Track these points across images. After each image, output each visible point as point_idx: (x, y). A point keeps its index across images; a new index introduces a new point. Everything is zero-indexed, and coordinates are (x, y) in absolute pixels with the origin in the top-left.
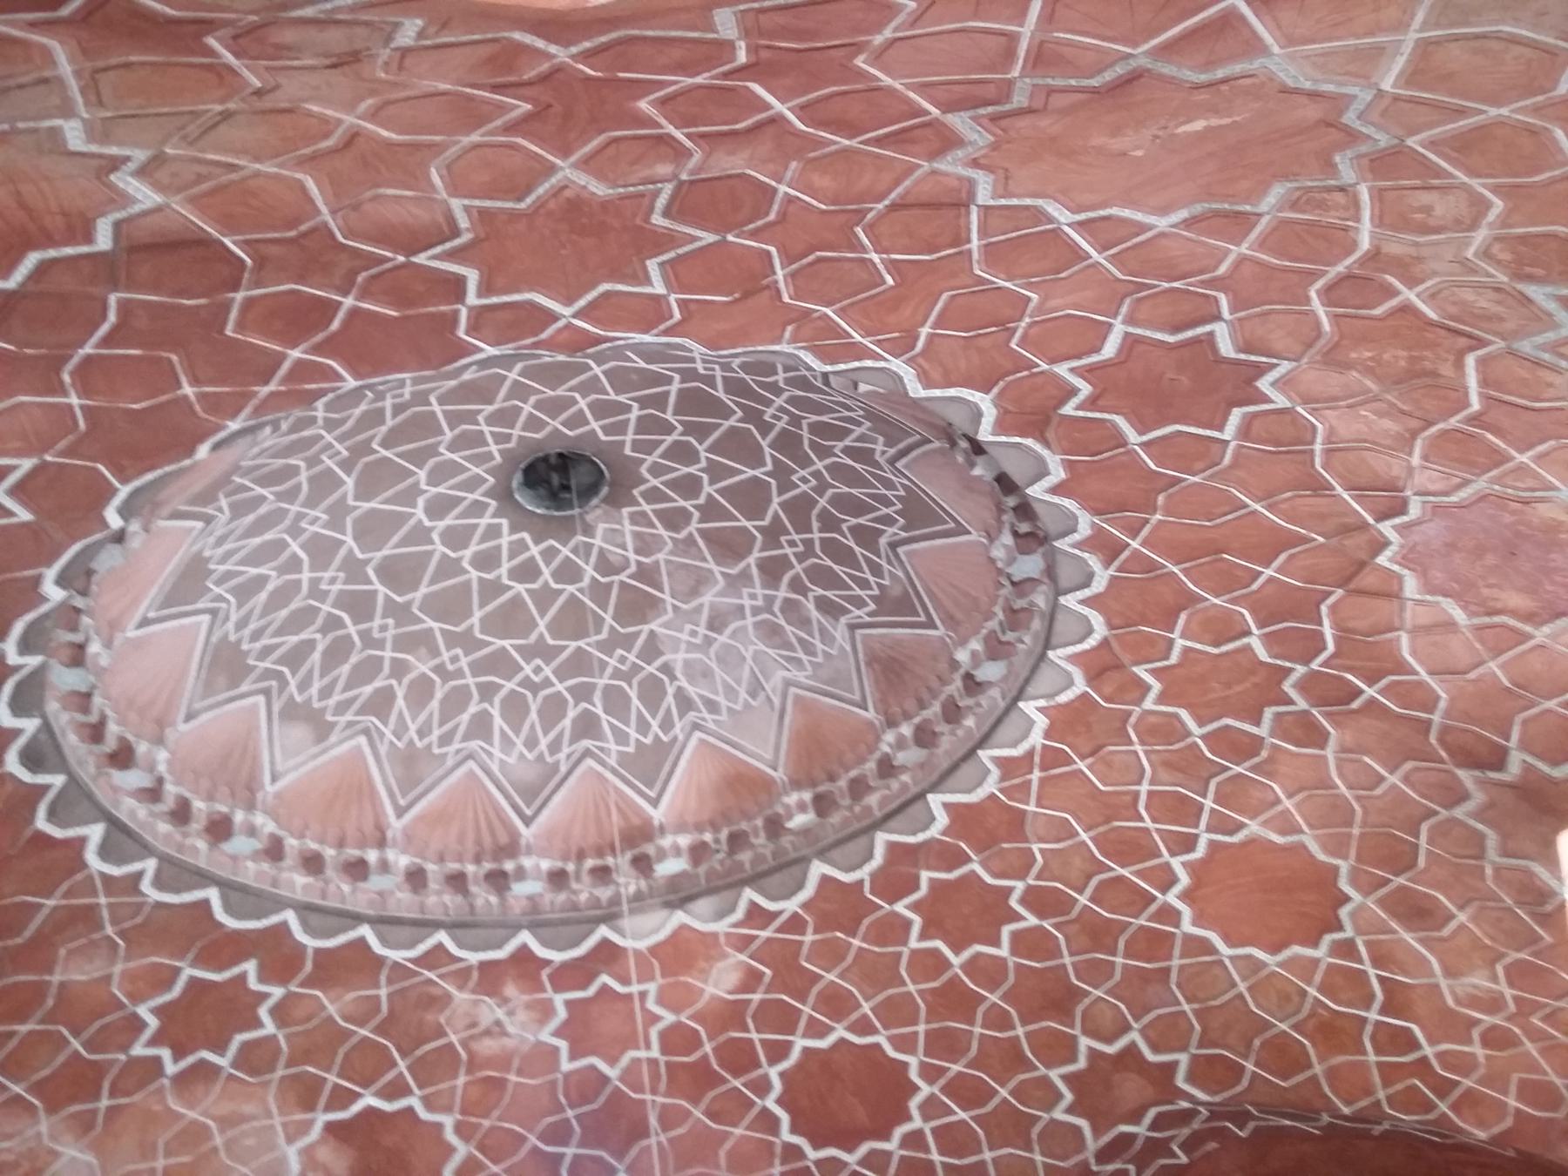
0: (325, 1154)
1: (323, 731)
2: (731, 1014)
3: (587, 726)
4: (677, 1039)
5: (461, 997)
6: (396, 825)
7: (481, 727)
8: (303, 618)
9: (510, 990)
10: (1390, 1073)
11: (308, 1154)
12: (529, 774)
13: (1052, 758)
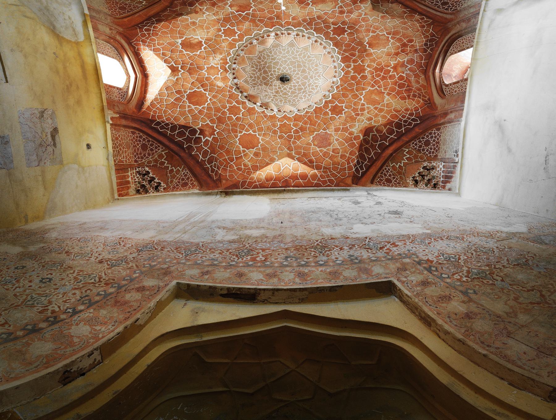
0: (197, 40)
1: (260, 52)
2: (212, 84)
3: (251, 77)
4: (208, 79)
5: (221, 56)
6: (245, 56)
7: (253, 67)
8: (275, 53)
9: (221, 61)
10: (225, 160)
11: (198, 39)
12: (246, 70)
13: (266, 116)
